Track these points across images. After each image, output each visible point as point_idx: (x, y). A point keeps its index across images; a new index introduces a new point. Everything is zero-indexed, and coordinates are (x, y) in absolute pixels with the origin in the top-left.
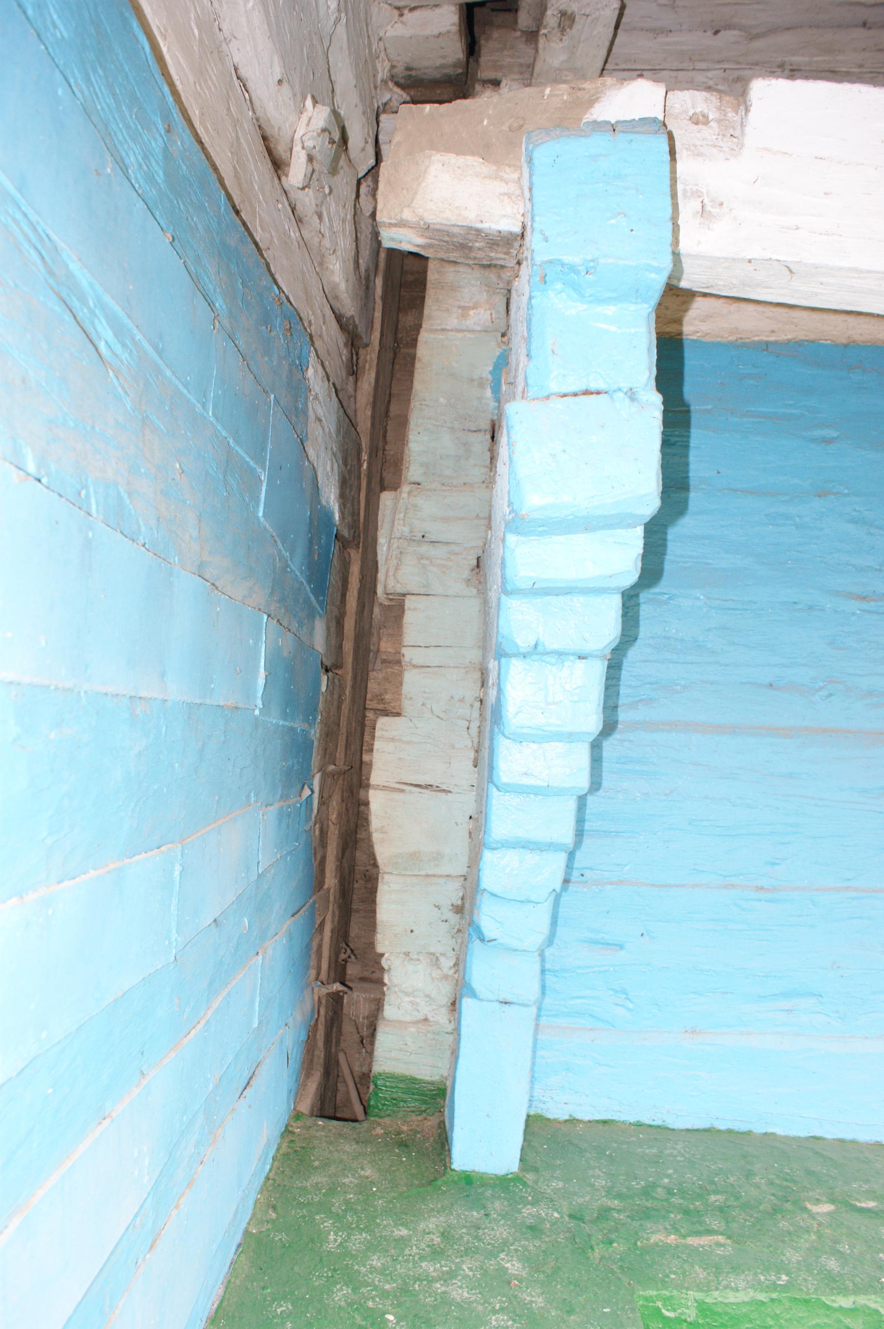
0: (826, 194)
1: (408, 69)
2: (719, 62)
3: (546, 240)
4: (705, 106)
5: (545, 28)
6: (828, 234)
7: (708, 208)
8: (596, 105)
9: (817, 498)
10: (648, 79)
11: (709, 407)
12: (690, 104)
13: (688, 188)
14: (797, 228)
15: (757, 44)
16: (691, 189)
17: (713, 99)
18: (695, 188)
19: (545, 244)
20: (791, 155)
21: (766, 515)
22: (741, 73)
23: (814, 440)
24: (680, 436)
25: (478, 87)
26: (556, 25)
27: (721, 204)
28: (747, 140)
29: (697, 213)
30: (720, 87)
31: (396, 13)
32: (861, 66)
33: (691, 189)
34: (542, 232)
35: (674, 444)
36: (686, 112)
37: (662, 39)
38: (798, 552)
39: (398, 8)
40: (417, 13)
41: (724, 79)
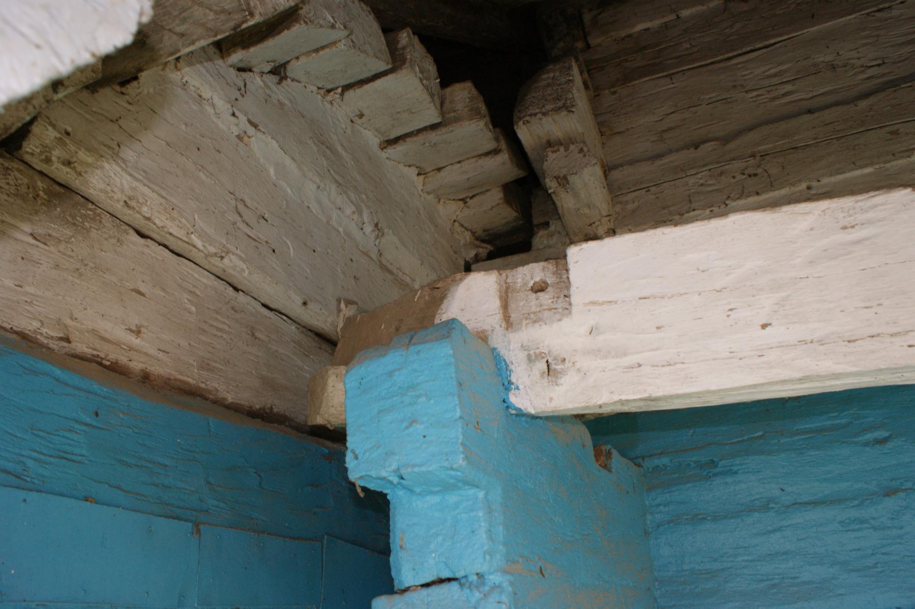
0: (658, 328)
1: (485, 231)
2: (704, 166)
3: (356, 458)
4: (542, 274)
5: (550, 188)
6: (670, 365)
7: (553, 366)
8: (445, 301)
9: (887, 499)
10: (479, 270)
11: (760, 433)
12: (528, 278)
13: (532, 352)
14: (640, 366)
15: (731, 146)
16: (535, 353)
17: (550, 266)
18: (538, 351)
19: (356, 462)
20: (616, 303)
21: (840, 522)
22: (723, 168)
23: (867, 444)
24: (740, 465)
25: (535, 229)
26: (557, 185)
27: (564, 360)
28: (574, 299)
29: (544, 373)
30: (709, 182)
31: (461, 203)
32: (815, 139)
33: (535, 353)
34: (353, 452)
35: (736, 473)
36: (526, 284)
37: (659, 162)
38: (883, 554)
39: (462, 200)
40: (475, 199)
41: (711, 176)
